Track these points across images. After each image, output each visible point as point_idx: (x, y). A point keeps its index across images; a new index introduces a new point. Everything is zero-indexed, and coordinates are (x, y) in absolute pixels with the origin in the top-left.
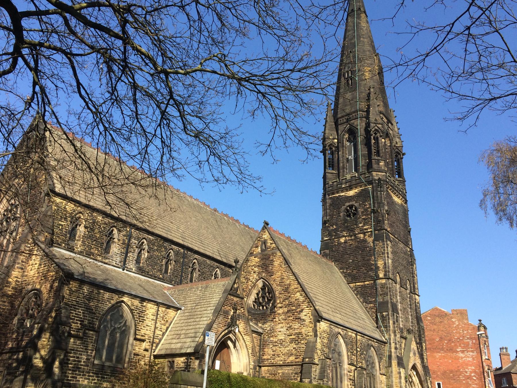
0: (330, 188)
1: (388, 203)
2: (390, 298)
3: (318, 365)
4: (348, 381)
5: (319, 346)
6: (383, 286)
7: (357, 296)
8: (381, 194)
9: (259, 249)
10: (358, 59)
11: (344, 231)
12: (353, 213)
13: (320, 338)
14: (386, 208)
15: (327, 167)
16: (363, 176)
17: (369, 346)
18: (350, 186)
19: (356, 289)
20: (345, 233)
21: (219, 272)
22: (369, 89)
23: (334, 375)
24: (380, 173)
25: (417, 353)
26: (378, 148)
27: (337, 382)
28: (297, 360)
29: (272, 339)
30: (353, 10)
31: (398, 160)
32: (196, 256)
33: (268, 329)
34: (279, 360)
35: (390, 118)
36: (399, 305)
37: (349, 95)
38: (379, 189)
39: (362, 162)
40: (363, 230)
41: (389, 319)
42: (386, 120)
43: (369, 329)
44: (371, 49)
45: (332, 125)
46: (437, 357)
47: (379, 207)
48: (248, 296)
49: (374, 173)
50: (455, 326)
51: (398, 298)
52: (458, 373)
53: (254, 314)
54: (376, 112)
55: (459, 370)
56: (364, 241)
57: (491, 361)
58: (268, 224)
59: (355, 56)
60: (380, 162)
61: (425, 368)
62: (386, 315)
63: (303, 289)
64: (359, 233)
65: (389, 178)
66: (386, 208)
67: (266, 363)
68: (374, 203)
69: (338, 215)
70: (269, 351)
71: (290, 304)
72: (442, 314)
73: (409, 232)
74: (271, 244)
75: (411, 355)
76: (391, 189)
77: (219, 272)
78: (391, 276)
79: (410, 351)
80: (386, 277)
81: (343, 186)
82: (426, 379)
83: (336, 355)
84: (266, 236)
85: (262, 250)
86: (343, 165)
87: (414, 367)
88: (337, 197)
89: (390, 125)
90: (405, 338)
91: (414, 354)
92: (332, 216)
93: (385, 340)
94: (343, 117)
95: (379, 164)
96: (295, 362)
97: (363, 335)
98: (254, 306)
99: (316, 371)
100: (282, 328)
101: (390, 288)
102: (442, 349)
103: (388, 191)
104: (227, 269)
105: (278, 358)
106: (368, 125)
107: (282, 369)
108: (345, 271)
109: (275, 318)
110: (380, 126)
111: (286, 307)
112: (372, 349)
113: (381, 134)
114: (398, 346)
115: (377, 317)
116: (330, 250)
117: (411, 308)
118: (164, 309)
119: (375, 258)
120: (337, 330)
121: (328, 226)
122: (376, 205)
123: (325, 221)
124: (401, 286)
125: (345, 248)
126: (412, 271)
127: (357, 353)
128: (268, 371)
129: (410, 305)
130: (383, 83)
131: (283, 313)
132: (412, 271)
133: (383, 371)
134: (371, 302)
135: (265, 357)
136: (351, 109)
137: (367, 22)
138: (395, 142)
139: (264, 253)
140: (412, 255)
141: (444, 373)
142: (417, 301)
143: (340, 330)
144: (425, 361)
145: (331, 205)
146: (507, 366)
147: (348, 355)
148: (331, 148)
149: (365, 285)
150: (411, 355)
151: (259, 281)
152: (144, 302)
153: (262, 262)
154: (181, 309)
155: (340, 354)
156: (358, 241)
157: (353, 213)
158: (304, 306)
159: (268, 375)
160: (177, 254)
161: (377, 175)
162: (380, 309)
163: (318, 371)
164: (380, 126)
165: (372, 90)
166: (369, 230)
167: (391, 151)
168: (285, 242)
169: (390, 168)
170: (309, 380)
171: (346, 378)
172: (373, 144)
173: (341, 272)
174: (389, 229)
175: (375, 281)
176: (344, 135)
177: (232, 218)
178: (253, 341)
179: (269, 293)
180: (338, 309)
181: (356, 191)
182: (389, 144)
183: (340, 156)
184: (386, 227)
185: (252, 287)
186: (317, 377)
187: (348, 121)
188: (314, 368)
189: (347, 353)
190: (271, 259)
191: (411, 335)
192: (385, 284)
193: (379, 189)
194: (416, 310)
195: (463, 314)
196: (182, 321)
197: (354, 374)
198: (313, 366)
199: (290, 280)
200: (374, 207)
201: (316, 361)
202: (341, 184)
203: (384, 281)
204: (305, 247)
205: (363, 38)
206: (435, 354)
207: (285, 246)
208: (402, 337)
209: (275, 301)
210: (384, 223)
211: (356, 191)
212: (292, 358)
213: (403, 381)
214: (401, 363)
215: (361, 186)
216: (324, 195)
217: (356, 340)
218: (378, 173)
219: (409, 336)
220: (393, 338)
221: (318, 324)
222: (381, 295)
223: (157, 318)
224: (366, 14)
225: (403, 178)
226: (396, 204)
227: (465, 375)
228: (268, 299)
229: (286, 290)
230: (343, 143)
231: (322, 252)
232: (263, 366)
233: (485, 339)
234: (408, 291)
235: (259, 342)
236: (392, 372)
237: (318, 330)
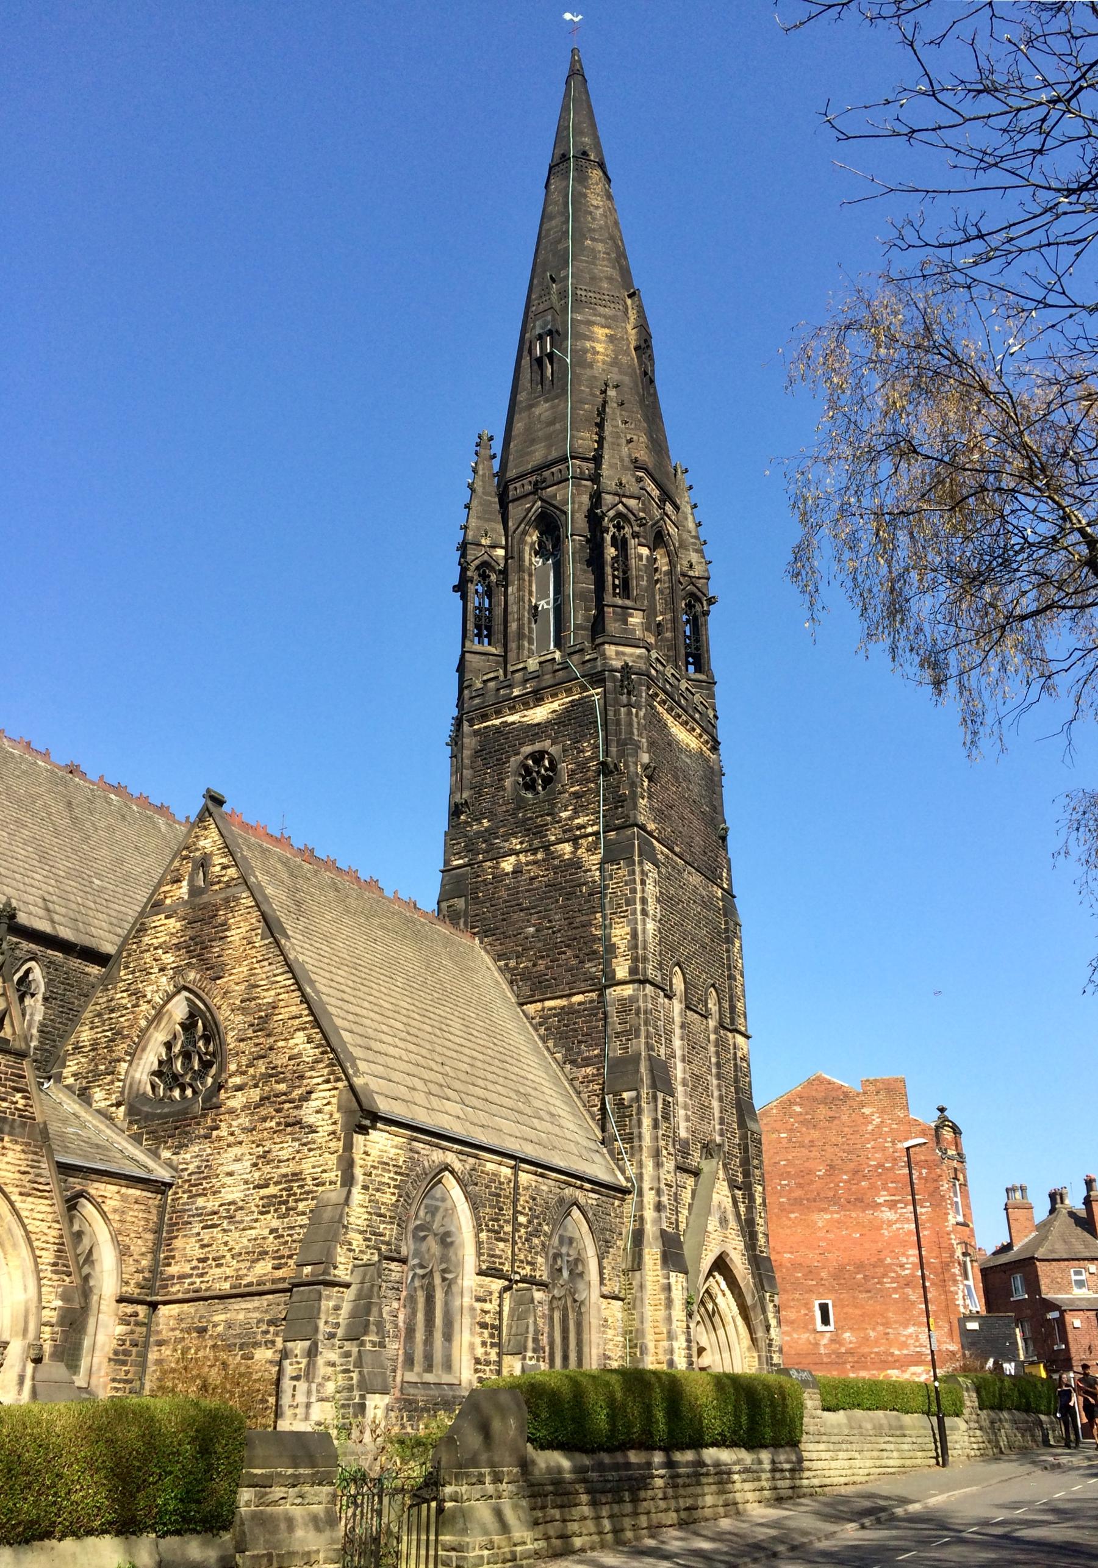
0: (477, 701)
1: (652, 744)
2: (647, 1043)
3: (347, 1286)
4: (472, 1333)
5: (357, 1215)
6: (626, 1006)
7: (544, 1042)
8: (630, 713)
9: (183, 890)
10: (575, 300)
11: (514, 834)
12: (544, 778)
13: (365, 1188)
14: (645, 758)
15: (469, 634)
16: (575, 657)
17: (566, 1206)
18: (535, 692)
19: (545, 1018)
20: (515, 843)
21: (37, 974)
22: (604, 392)
23: (420, 1316)
25: (731, 1217)
26: (625, 572)
27: (428, 1341)
28: (279, 1273)
29: (200, 1202)
30: (564, 158)
31: (696, 619)
33: (192, 1168)
34: (218, 1280)
35: (671, 488)
36: (680, 1066)
37: (543, 409)
38: (624, 698)
39: (577, 616)
40: (570, 830)
42: (656, 493)
43: (572, 1147)
44: (616, 275)
45: (491, 503)
46: (820, 1224)
47: (622, 754)
48: (133, 1054)
50: (870, 1127)
51: (677, 1043)
52: (880, 1270)
53: (149, 1117)
54: (622, 460)
55: (881, 1261)
56: (575, 864)
57: (972, 1230)
58: (219, 802)
59: (566, 291)
60: (631, 616)
61: (759, 1264)
62: (632, 1100)
63: (316, 1020)
65: (660, 667)
66: (645, 758)
67: (174, 1289)
68: (607, 743)
69: (501, 785)
70: (187, 1246)
71: (274, 1074)
72: (834, 1094)
73: (724, 839)
74: (224, 868)
75: (713, 1224)
76: (664, 702)
77: (37, 974)
78: (651, 973)
79: (709, 1213)
80: (638, 979)
81: (516, 692)
82: (762, 1299)
83: (432, 1245)
84: (209, 841)
85: (194, 891)
86: (520, 627)
87: (721, 1265)
88: (497, 730)
89: (669, 507)
90: (696, 1173)
91: (723, 1221)
92: (477, 790)
93: (624, 1183)
94: (521, 477)
95: (626, 623)
96: (274, 1282)
97: (542, 1168)
98: (153, 1087)
99: (337, 1308)
100: (237, 1160)
101: (646, 1012)
102: (835, 1200)
103: (653, 707)
104: (75, 963)
105: (218, 1271)
106: (596, 498)
107: (226, 1310)
108: (512, 963)
109: (217, 1128)
110: (632, 503)
111: (256, 1086)
112: (576, 1213)
113: (637, 529)
114: (665, 1199)
115: (603, 1109)
116: (470, 901)
117: (719, 1076)
119: (604, 917)
120: (438, 1156)
121: (466, 822)
122: (613, 750)
123: (456, 805)
124: (688, 1007)
125: (514, 892)
126: (728, 958)
127: (515, 1230)
128: (180, 1319)
129: (718, 1065)
130: (652, 381)
131: (246, 1107)
132: (728, 958)
133: (614, 1286)
134: (587, 1062)
135: (173, 1270)
136: (550, 453)
137: (609, 197)
138: (685, 563)
139: (197, 900)
140: (729, 910)
141: (839, 1273)
142: (739, 1054)
143: (451, 1158)
144: (762, 1240)
145: (477, 753)
146: (1026, 1240)
147: (479, 1244)
148: (484, 577)
149: (571, 1005)
150: (713, 1224)
151: (177, 998)
153: (189, 932)
155: (446, 1240)
156: (555, 867)
157: (544, 778)
158: (315, 1078)
159: (177, 1332)
161: (618, 653)
162: (613, 1076)
163: (345, 1312)
164: (632, 503)
165: (612, 393)
166: (590, 830)
167: (672, 589)
168: (285, 864)
169: (667, 640)
170: (307, 1343)
171: (467, 1321)
172: (608, 559)
173: (500, 968)
174: (651, 826)
175: (601, 990)
176: (525, 533)
177: (144, 801)
179: (207, 1040)
180: (457, 1085)
181: (555, 706)
182: (665, 568)
183: (511, 599)
184: (641, 819)
185: (150, 1023)
186: (340, 1332)
187: (537, 487)
188: (329, 1298)
189: (477, 1236)
190: (220, 919)
191: (714, 1161)
192: (633, 999)
193: (624, 698)
194: (736, 1081)
195: (893, 1092)
197: (500, 1305)
198: (326, 1291)
199: (274, 987)
200: (607, 753)
201: (342, 1273)
202: (510, 686)
203: (628, 990)
204: (373, 884)
205: (593, 239)
206: (815, 1216)
207: (285, 876)
208: (680, 1168)
209: (222, 1068)
210: (635, 807)
211: (555, 706)
212: (264, 1268)
213: (678, 1312)
214: (673, 1255)
215: (569, 692)
216: (458, 722)
217: (516, 1187)
218: (621, 649)
219: (707, 1166)
220: (652, 1173)
221: (358, 1139)
222: (618, 1035)
224: (605, 173)
225: (709, 672)
226: (681, 750)
227: (899, 1276)
229: (263, 1024)
230: (521, 559)
231: (444, 905)
232: (165, 1303)
233: (955, 1164)
234: (712, 1023)
235: (154, 1218)
236: (642, 1287)
237: (358, 1162)
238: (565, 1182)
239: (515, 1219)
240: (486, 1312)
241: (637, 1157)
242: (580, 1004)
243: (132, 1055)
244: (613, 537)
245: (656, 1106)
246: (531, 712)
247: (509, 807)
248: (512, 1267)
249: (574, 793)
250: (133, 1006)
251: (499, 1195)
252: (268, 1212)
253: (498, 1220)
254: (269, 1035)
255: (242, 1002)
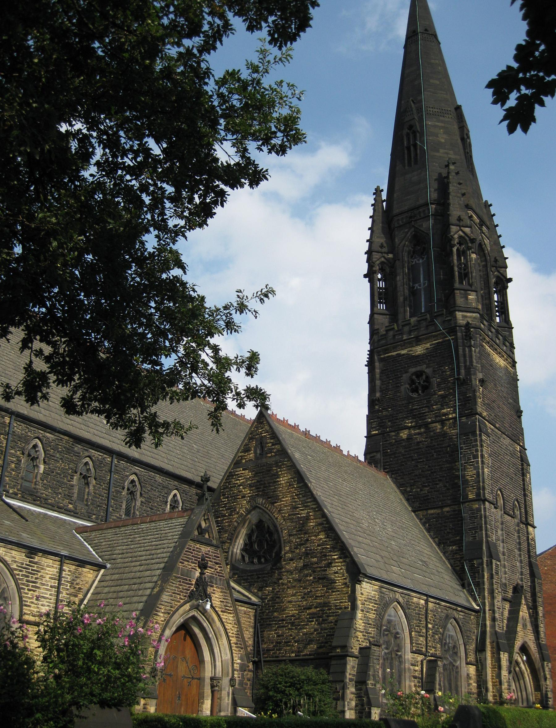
0: (383, 342)
4: (410, 681)
9: (252, 456)
24: (469, 314)
32: (136, 469)
41: (483, 571)
49: (459, 315)
64: (433, 422)
81: (405, 337)
85: (256, 458)
87: (524, 649)
91: (525, 626)
95: (467, 299)
110: (467, 230)
117: (520, 550)
118: (74, 567)
122: (463, 371)
140: (524, 461)
142: (530, 537)
143: (398, 596)
152: (35, 554)
154: (105, 567)
160: (98, 465)
164: (467, 230)
165: (452, 167)
166: (450, 416)
171: (407, 674)
174: (485, 414)
178: (238, 622)
181: (428, 345)
194: (529, 551)
196: (106, 590)
197: (422, 668)
202: (402, 334)
211: (428, 345)
223: (59, 584)
228: (268, 544)
231: (368, 457)
238: (449, 607)
239: (427, 625)
240: (416, 671)
241: (482, 594)
242: (447, 512)
243: (231, 540)
244: (458, 250)
245: (492, 567)
246: (414, 349)
247: (403, 402)
248: (426, 649)
249: (441, 395)
250: (230, 515)
251: (419, 614)
252: (313, 621)
253: (419, 626)
254: (306, 533)
255: (289, 515)
